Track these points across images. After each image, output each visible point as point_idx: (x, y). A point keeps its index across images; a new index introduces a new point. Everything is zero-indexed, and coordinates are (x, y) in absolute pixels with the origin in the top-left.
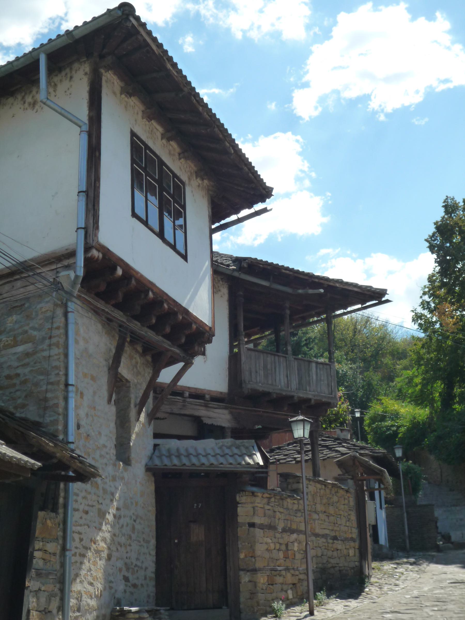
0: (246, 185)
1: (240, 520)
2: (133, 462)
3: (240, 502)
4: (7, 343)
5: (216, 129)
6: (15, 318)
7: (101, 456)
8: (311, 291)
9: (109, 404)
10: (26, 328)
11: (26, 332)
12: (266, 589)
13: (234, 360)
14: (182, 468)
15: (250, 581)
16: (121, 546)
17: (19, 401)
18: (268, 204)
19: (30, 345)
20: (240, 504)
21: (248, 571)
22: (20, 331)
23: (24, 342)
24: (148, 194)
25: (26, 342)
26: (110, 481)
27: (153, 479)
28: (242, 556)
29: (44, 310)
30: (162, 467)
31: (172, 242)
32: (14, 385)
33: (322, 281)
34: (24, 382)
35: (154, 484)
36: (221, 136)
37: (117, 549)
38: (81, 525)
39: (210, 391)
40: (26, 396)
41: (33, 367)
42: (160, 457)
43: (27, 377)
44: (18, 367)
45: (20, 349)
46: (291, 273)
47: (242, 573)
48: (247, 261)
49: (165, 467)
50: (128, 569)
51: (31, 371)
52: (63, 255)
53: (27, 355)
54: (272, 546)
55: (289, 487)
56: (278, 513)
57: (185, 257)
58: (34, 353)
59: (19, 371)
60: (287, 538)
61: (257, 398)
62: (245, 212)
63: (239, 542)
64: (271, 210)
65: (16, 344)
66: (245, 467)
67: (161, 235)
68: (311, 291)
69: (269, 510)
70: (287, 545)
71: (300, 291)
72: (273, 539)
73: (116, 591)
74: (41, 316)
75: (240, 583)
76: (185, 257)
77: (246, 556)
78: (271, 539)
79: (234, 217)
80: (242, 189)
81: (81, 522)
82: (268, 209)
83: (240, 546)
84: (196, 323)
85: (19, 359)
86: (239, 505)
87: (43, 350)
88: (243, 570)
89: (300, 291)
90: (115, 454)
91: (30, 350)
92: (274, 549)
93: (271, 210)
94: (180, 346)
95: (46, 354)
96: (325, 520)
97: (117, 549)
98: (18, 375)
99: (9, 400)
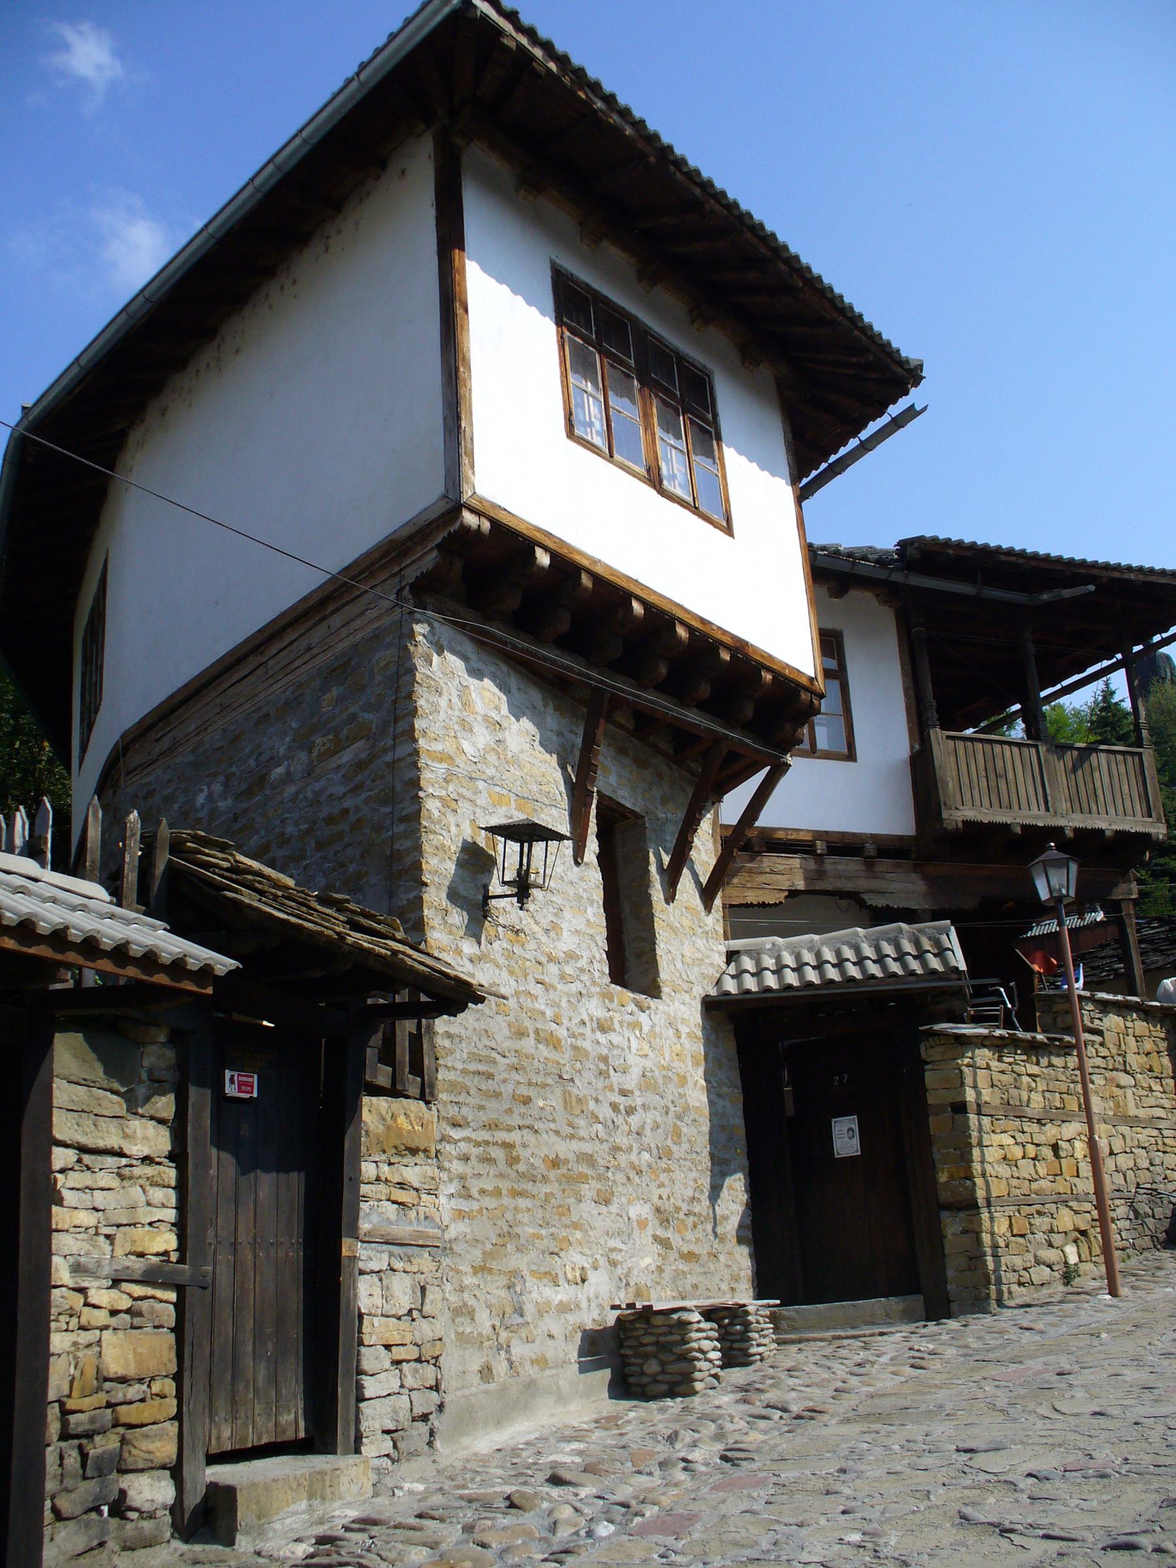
0: (854, 360)
1: (931, 1099)
2: (665, 990)
3: (929, 1060)
4: (323, 748)
5: (749, 236)
6: (335, 692)
7: (563, 977)
8: (1067, 593)
9: (577, 864)
10: (354, 709)
11: (354, 717)
12: (1007, 1246)
13: (921, 766)
14: (784, 994)
15: (965, 1232)
16: (639, 1173)
17: (352, 868)
18: (915, 397)
19: (359, 745)
20: (928, 1063)
21: (959, 1210)
22: (344, 716)
23: (351, 740)
24: (610, 394)
25: (355, 740)
26: (593, 1031)
27: (730, 1027)
28: (943, 1178)
29: (382, 664)
30: (740, 997)
31: (690, 499)
32: (341, 835)
33: (1095, 572)
34: (357, 826)
35: (733, 1038)
36: (763, 250)
37: (629, 1179)
38: (509, 1129)
39: (873, 837)
40: (362, 856)
41: (371, 790)
42: (737, 976)
43: (361, 814)
44: (345, 795)
45: (346, 757)
46: (1021, 561)
47: (945, 1215)
48: (916, 545)
49: (748, 996)
50: (665, 1222)
51: (367, 801)
52: (410, 538)
53: (360, 765)
54: (1018, 1152)
55: (1059, 1020)
56: (1025, 1079)
57: (728, 530)
58: (372, 757)
59: (347, 804)
60: (1051, 1132)
61: (982, 839)
62: (873, 427)
63: (935, 1150)
64: (925, 409)
65: (338, 747)
66: (927, 981)
67: (654, 479)
68: (1067, 593)
69: (1002, 1072)
70: (1055, 1148)
71: (1045, 597)
72: (1018, 1135)
73: (630, 1270)
74: (378, 678)
75: (943, 1237)
76: (728, 530)
77: (951, 1177)
78: (1013, 1137)
79: (853, 443)
80: (852, 372)
81: (515, 1120)
82: (918, 408)
83: (936, 1156)
84: (769, 670)
85: (346, 778)
86: (927, 1067)
87: (385, 751)
88: (948, 1207)
89: (1045, 597)
90: (607, 972)
91: (363, 755)
92: (1024, 1157)
93: (925, 409)
94: (747, 728)
95: (388, 758)
96: (1150, 1087)
97: (629, 1179)
98: (345, 812)
99: (334, 869)
